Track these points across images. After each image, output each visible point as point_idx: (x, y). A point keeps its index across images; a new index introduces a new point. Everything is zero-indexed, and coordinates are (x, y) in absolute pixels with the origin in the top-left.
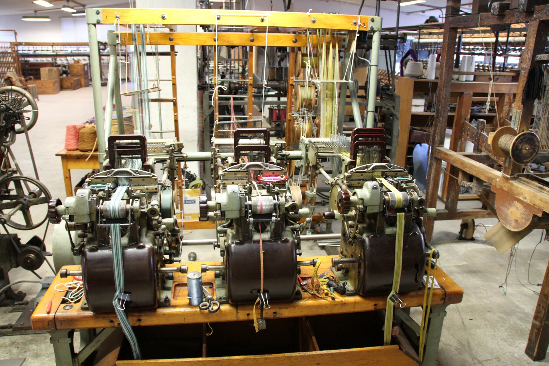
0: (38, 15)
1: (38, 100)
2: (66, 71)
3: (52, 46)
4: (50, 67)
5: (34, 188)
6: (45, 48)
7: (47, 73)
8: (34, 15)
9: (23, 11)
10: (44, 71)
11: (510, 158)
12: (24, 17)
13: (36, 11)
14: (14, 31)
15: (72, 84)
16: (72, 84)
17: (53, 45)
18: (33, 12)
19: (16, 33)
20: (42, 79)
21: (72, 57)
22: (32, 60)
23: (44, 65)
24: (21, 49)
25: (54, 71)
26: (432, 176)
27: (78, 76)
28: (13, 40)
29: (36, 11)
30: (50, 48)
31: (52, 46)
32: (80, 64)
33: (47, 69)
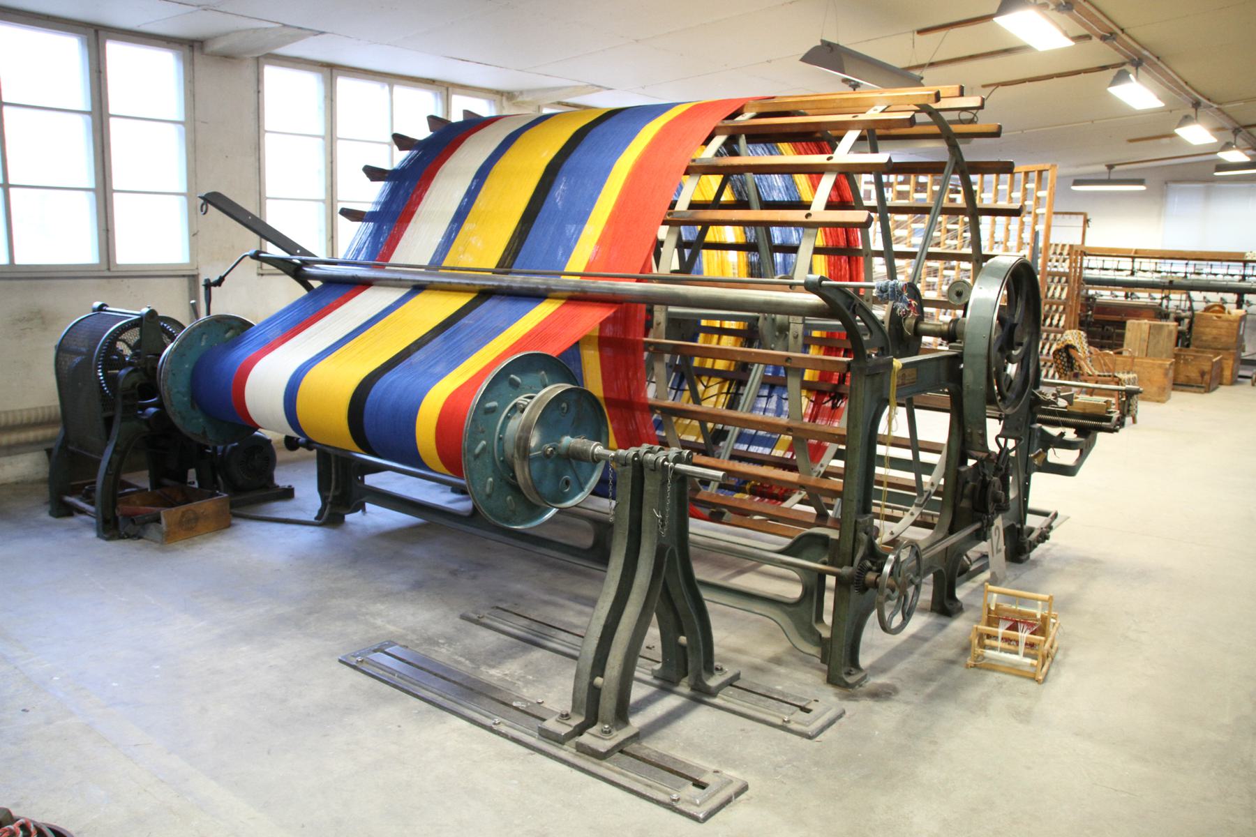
0: (1113, 177)
1: (1134, 421)
2: (1187, 335)
3: (1133, 258)
4: (1149, 318)
5: (133, 336)
6: (1110, 263)
7: (1145, 335)
8: (1105, 177)
9: (1077, 166)
10: (1136, 329)
11: (809, 525)
12: (1077, 183)
13: (1110, 167)
14: (1085, 215)
15: (1203, 374)
16: (1203, 374)
17: (1135, 255)
18: (1104, 168)
19: (1086, 221)
20: (1127, 350)
21: (1204, 294)
22: (1105, 295)
23: (1137, 312)
24: (1094, 267)
25: (1165, 332)
26: (1003, 655)
27: (1216, 351)
28: (1078, 242)
29: (1110, 167)
30: (1126, 264)
31: (1133, 258)
32: (1225, 316)
33: (1145, 323)
